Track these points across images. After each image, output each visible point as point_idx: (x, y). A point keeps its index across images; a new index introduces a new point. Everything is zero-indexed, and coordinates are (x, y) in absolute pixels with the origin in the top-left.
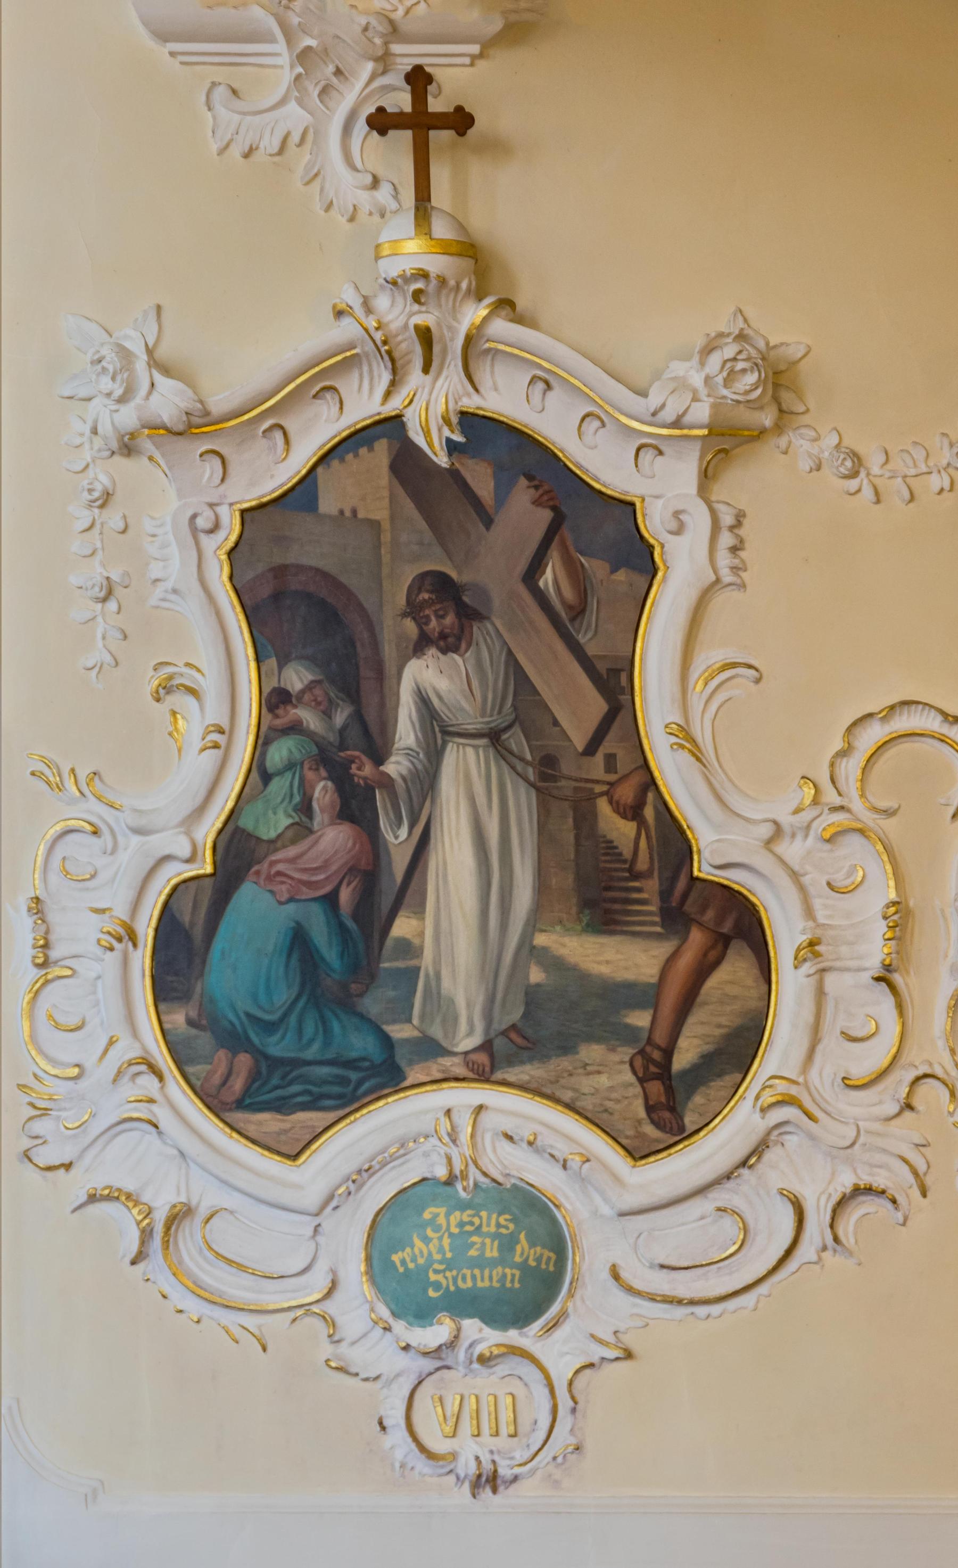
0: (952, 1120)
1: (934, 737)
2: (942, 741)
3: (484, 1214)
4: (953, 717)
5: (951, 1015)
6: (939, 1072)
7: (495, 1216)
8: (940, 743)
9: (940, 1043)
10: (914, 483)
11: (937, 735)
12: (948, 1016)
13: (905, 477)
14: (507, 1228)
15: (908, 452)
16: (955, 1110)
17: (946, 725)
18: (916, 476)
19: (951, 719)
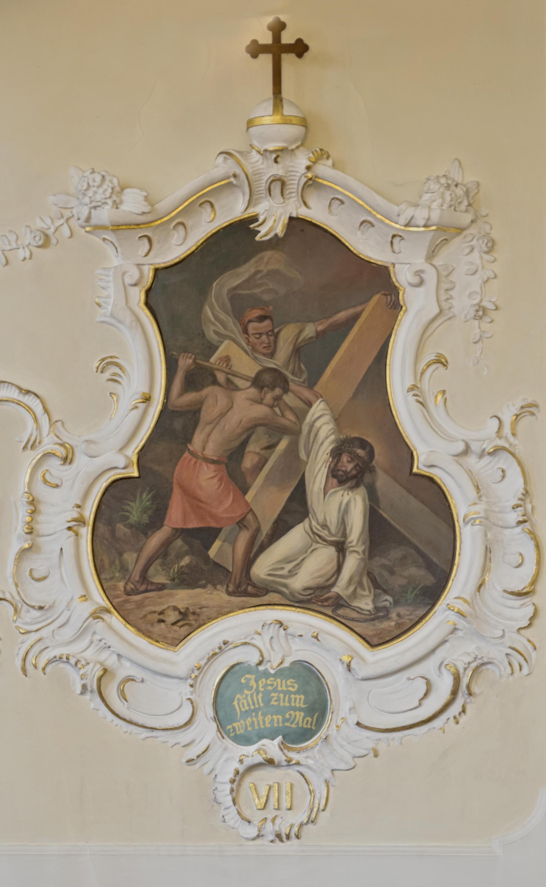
0: (15, 625)
1: (13, 402)
2: (19, 404)
3: (279, 680)
4: (25, 390)
5: (16, 564)
6: (8, 597)
7: (284, 681)
8: (17, 405)
9: (10, 580)
10: (8, 254)
11: (16, 401)
12: (15, 565)
13: (3, 251)
14: (293, 687)
15: (5, 236)
16: (16, 619)
17: (22, 395)
18: (10, 250)
19: (23, 391)
